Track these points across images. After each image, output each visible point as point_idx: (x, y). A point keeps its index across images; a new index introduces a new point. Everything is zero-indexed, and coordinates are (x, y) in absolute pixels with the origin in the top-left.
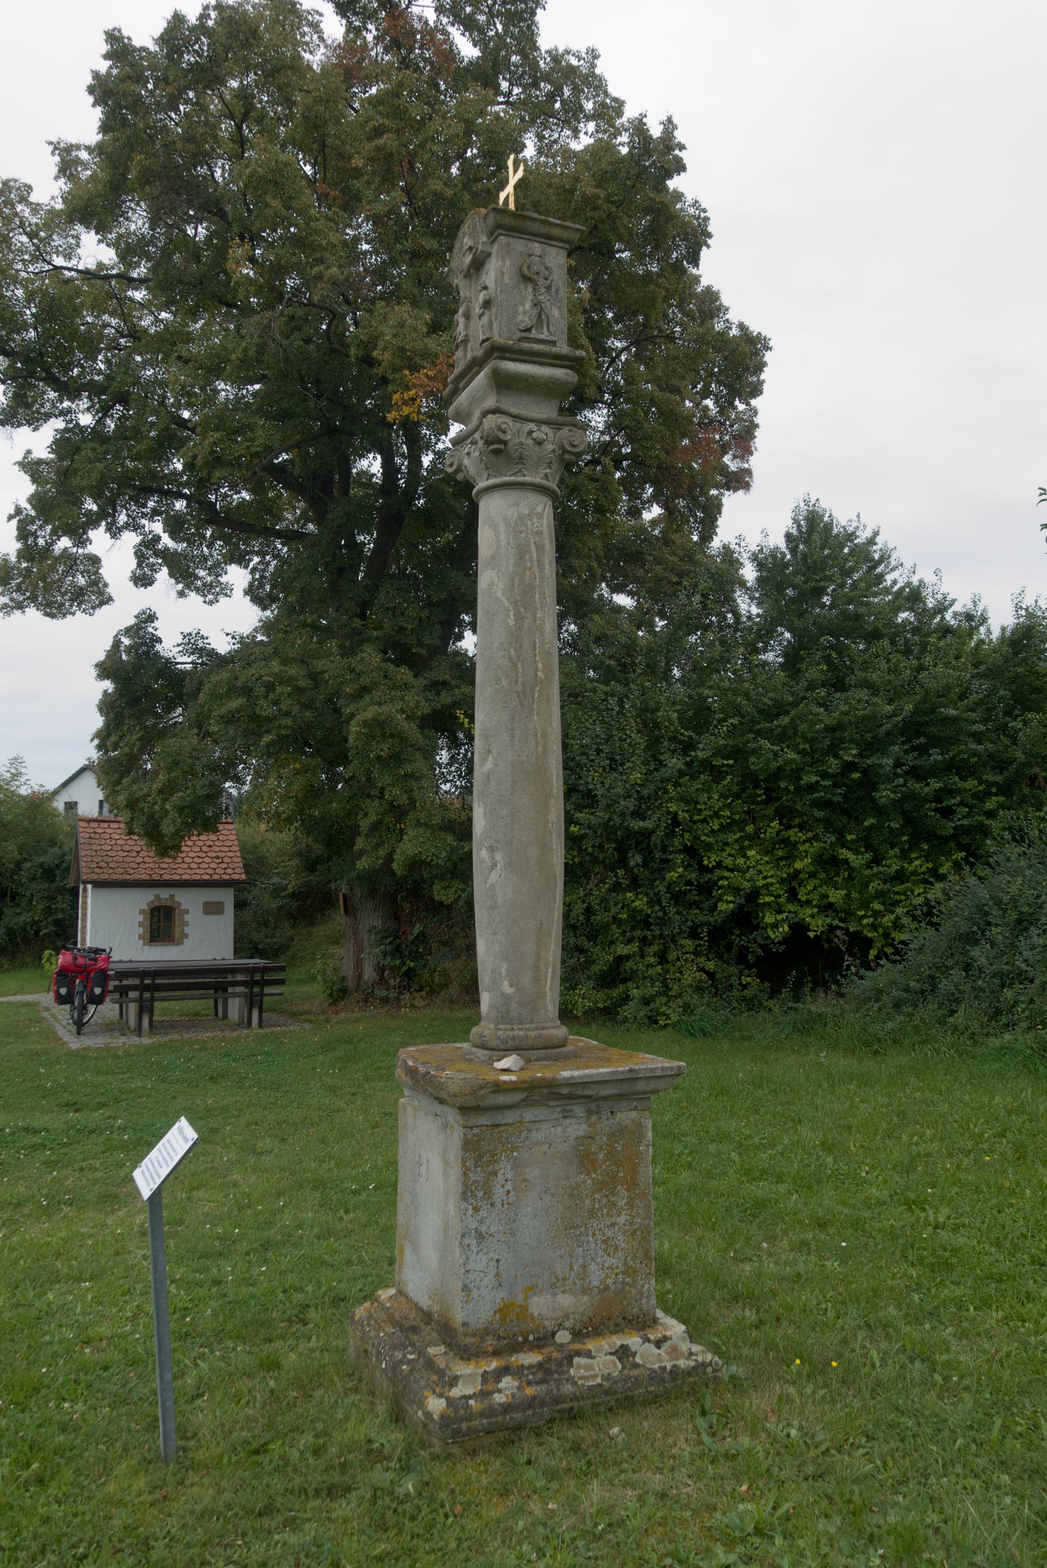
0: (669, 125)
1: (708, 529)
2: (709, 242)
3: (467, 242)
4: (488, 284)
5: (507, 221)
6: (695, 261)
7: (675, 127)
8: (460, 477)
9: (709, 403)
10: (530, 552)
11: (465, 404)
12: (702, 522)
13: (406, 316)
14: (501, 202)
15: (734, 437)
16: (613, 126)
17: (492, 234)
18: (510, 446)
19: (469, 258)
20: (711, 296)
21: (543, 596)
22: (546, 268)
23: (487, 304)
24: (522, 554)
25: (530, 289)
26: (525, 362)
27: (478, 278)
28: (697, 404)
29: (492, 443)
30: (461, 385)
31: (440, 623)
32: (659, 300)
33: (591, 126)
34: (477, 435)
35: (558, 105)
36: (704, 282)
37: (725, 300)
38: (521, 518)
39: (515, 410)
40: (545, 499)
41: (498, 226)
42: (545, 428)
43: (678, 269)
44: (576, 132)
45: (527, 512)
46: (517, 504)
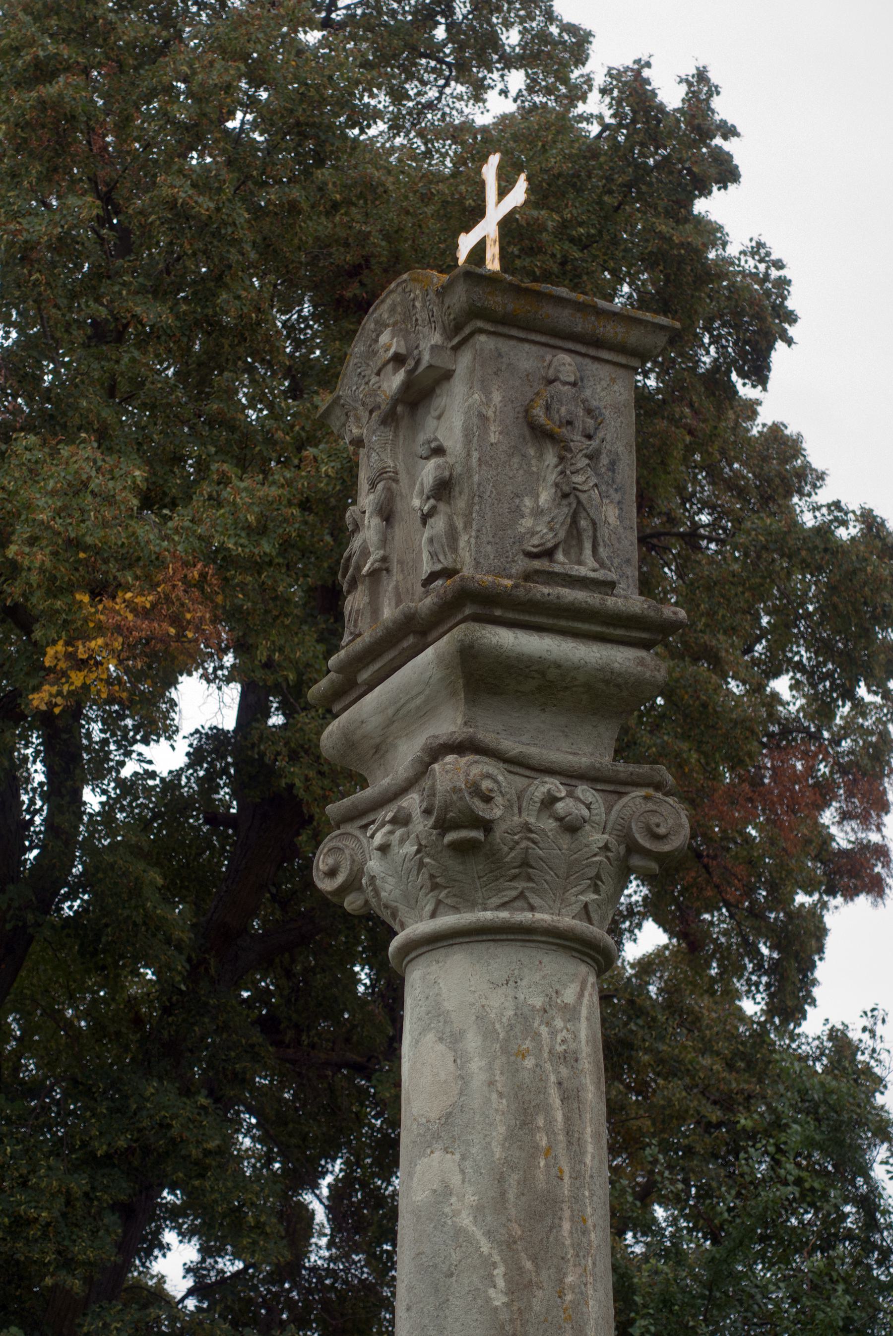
0: (700, 86)
1: (792, 992)
2: (792, 331)
3: (389, 342)
4: (447, 444)
5: (498, 302)
6: (759, 373)
7: (714, 90)
8: (352, 903)
9: (781, 685)
10: (545, 1108)
11: (374, 723)
12: (775, 969)
13: (88, 470)
14: (463, 254)
15: (844, 770)
16: (565, 81)
17: (458, 328)
18: (499, 832)
19: (395, 381)
20: (782, 446)
21: (579, 1220)
22: (589, 411)
23: (443, 489)
24: (525, 1114)
25: (551, 458)
26: (539, 629)
27: (415, 426)
28: (757, 689)
29: (456, 826)
30: (364, 676)
31: (115, 1207)
32: (677, 453)
33: (517, 79)
34: (413, 802)
35: (440, 33)
36: (766, 416)
37: (816, 455)
38: (523, 1018)
39: (511, 746)
40: (583, 969)
41: (475, 312)
42: (584, 791)
43: (717, 385)
44: (478, 92)
45: (538, 1002)
46: (513, 981)
